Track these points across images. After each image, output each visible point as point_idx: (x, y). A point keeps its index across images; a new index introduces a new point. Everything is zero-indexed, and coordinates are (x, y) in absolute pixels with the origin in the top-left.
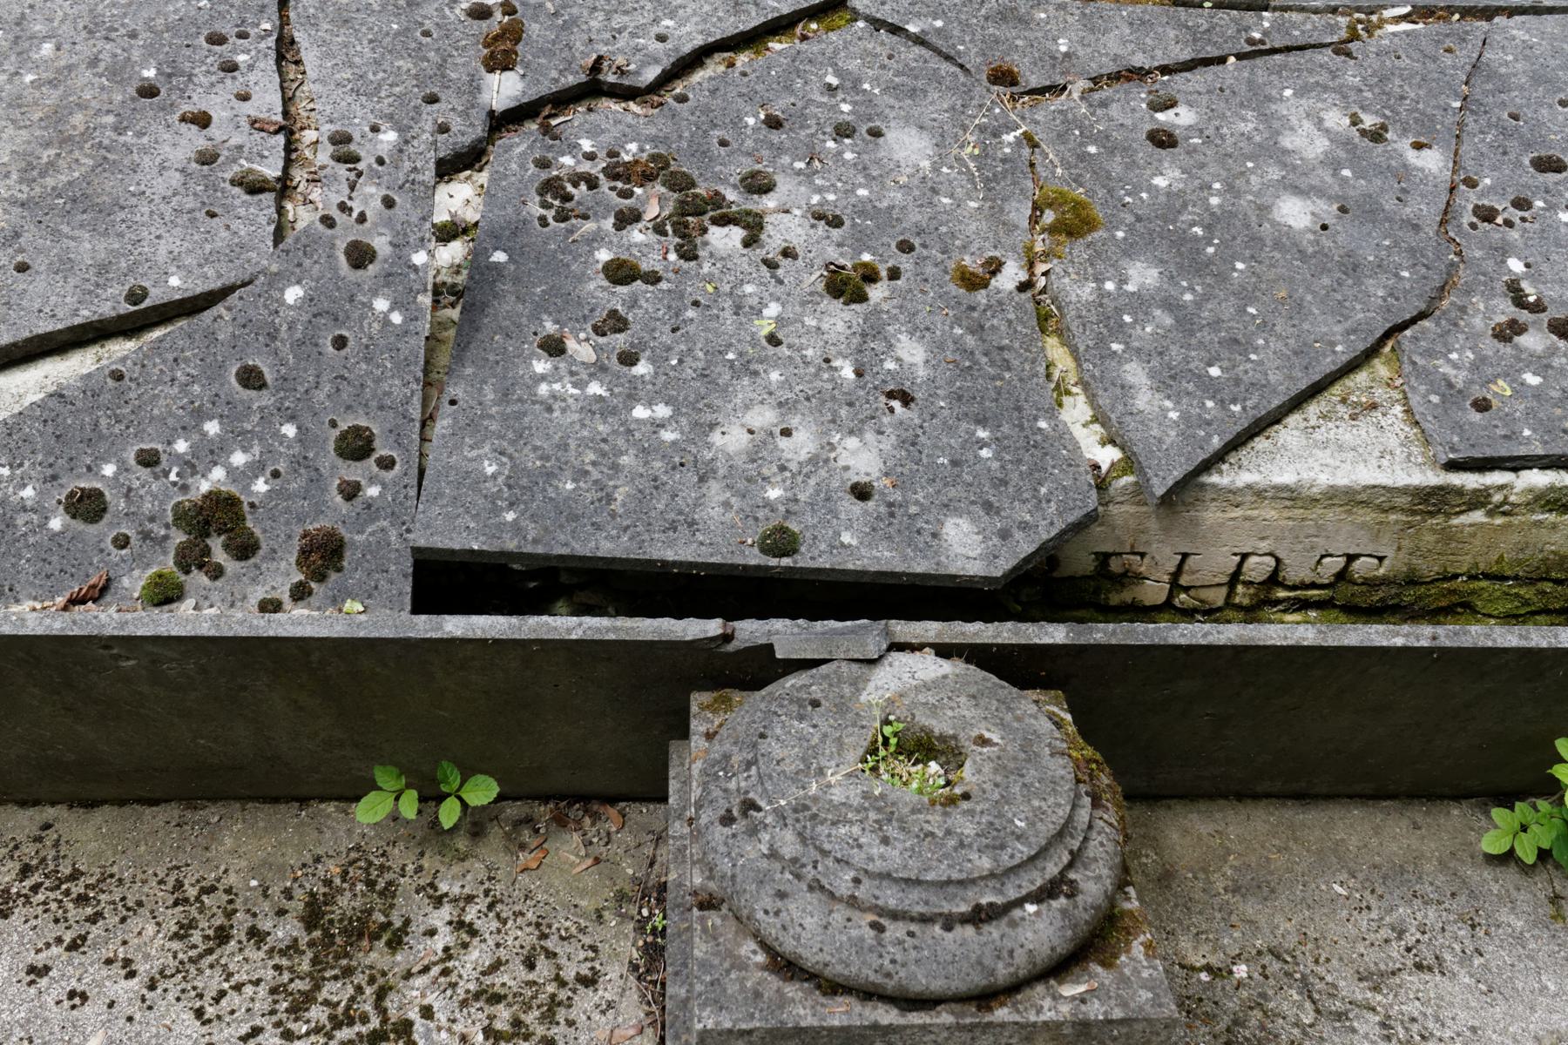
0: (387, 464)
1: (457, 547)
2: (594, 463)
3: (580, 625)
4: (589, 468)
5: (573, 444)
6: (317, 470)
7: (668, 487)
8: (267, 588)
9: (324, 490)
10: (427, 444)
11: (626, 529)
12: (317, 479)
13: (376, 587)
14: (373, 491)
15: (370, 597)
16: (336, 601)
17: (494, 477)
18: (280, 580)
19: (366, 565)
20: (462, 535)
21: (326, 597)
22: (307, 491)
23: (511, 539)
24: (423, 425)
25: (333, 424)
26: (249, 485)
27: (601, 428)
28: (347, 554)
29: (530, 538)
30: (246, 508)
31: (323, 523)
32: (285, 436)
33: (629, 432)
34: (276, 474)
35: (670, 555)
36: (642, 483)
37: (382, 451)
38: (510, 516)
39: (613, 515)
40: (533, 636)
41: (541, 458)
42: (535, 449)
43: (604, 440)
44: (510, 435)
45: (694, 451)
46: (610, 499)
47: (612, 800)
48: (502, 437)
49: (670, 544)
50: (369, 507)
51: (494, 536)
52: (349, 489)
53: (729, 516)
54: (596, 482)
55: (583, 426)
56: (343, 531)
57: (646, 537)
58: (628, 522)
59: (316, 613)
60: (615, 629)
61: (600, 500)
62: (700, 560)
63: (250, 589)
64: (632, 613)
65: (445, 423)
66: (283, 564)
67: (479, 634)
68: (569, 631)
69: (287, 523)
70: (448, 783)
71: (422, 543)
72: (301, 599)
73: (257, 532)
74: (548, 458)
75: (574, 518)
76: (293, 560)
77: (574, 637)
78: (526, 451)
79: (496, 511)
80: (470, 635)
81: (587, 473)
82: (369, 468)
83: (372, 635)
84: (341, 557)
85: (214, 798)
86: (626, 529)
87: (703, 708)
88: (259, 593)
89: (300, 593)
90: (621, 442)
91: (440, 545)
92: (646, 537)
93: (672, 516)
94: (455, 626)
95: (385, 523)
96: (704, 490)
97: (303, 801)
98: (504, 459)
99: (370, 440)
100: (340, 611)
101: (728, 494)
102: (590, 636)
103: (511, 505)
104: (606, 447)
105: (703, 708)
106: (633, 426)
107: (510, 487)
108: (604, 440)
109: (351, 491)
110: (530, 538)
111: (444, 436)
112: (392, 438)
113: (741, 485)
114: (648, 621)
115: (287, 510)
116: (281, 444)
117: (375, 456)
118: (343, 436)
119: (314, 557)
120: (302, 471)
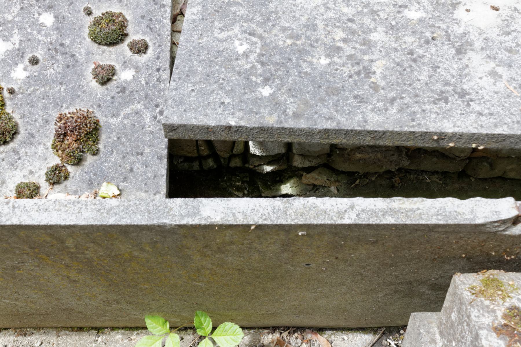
0: (140, 48)
1: (212, 123)
2: (345, 40)
3: (352, 207)
4: (341, 44)
5: (320, 25)
6: (73, 56)
7: (426, 60)
8: (25, 172)
9: (81, 75)
10: (177, 35)
11: (392, 101)
12: (72, 65)
13: (131, 170)
14: (125, 75)
15: (125, 179)
16: (92, 185)
17: (246, 55)
18: (37, 164)
19: (121, 147)
20: (214, 111)
21: (82, 180)
22: (63, 76)
23: (270, 114)
24: (174, 20)
25: (89, 13)
26: (9, 72)
27: (345, 10)
28: (103, 137)
29: (290, 112)
30: (6, 94)
31: (80, 106)
32: (42, 24)
33: (373, 12)
34: (34, 61)
35: (448, 127)
36: (398, 57)
37: (135, 35)
38: (266, 91)
39: (375, 87)
40: (301, 221)
41: (291, 37)
42: (284, 29)
43: (351, 20)
44: (258, 18)
45: (443, 26)
46: (368, 73)
47: (320, 330)
48: (251, 20)
49: (446, 115)
50: (123, 90)
51: (251, 111)
52: (103, 74)
53: (500, 86)
54: (350, 57)
55: (328, 9)
56: (98, 115)
57: (416, 108)
58: (393, 94)
59: (73, 198)
60: (393, 212)
61: (358, 73)
62: (484, 131)
63: (8, 174)
64: (463, 194)
65: (194, 10)
66: (41, 148)
67: (240, 220)
68: (341, 214)
69: (45, 108)
70: (203, 329)
71: (175, 120)
72: (58, 182)
73: (16, 117)
74: (298, 37)
75: (336, 91)
76: (49, 144)
77: (347, 221)
78: (274, 32)
79: (251, 87)
80: (231, 221)
81: (339, 49)
82: (122, 53)
83: (123, 222)
84: (96, 141)
85: (38, 328)
86: (392, 101)
87: (476, 293)
88: (17, 178)
89: (57, 177)
90: (367, 21)
91: (194, 122)
92: (416, 108)
93: (438, 87)
94: (214, 210)
95: (139, 106)
96: (465, 61)
97: (99, 330)
98: (254, 39)
99: (123, 25)
100: (96, 195)
101: (492, 65)
102: (364, 220)
103: (266, 81)
104: (354, 26)
105: (476, 293)
106: (375, 8)
107: (263, 64)
108: (351, 20)
109: (106, 76)
110: (290, 112)
111: (194, 21)
112: (145, 22)
113: (503, 55)
114: (429, 202)
115: (45, 96)
116: (39, 32)
117: (128, 41)
118: (97, 22)
119: (69, 140)
120: (59, 57)
